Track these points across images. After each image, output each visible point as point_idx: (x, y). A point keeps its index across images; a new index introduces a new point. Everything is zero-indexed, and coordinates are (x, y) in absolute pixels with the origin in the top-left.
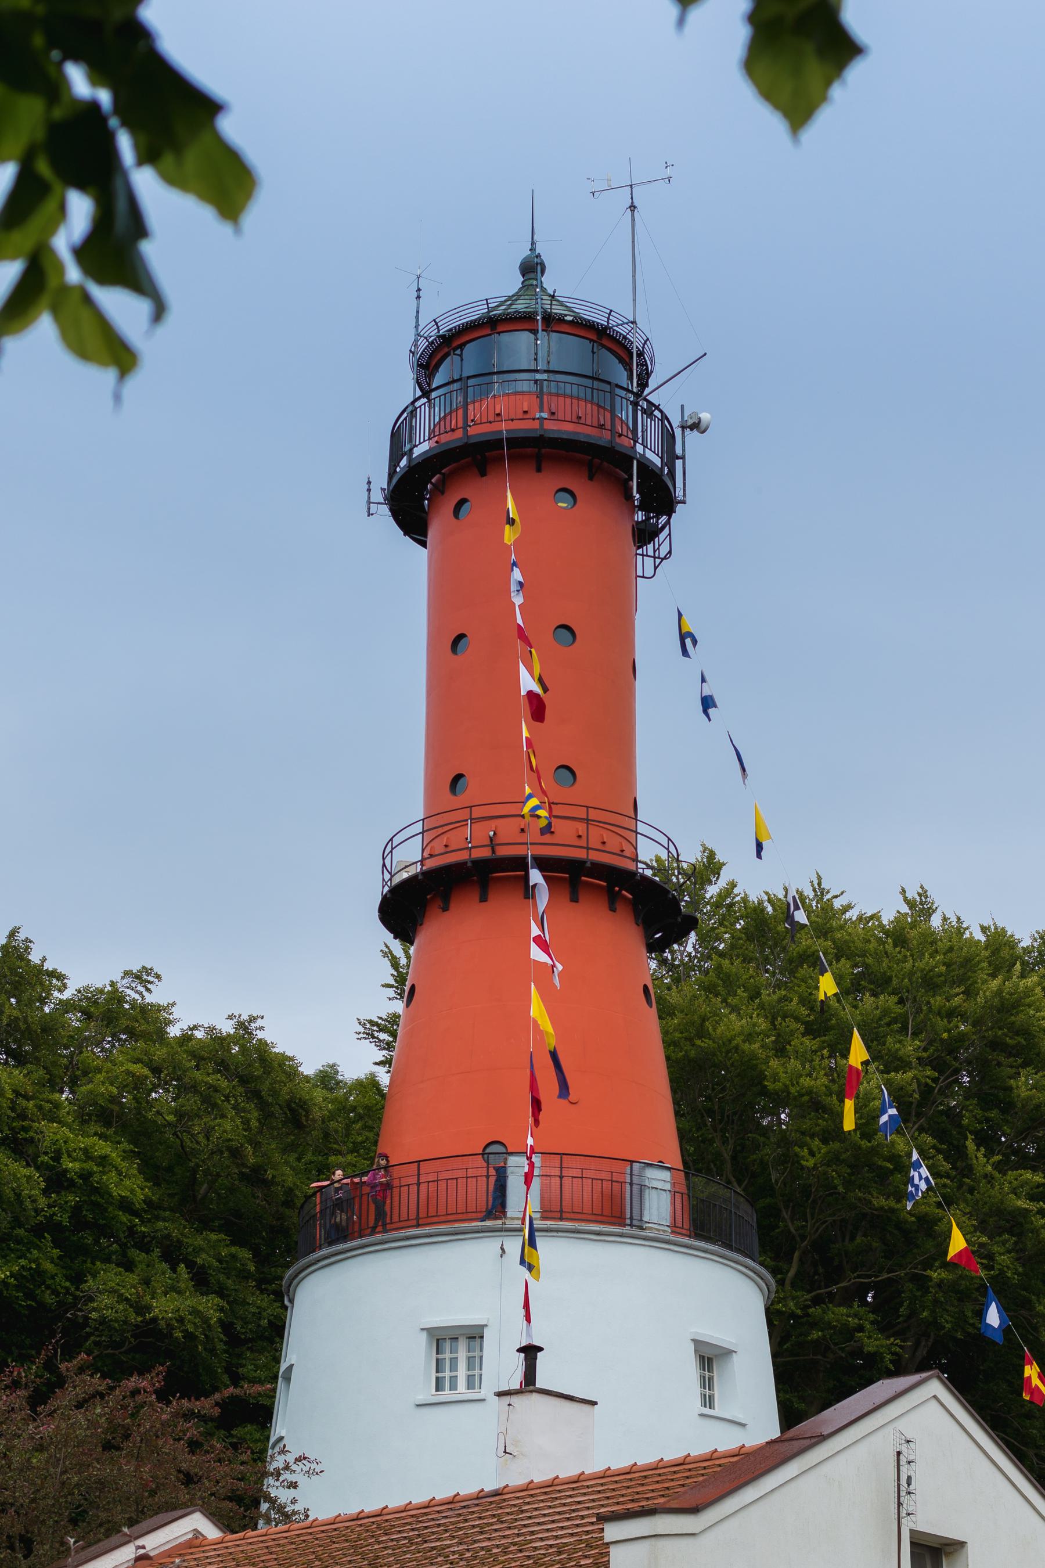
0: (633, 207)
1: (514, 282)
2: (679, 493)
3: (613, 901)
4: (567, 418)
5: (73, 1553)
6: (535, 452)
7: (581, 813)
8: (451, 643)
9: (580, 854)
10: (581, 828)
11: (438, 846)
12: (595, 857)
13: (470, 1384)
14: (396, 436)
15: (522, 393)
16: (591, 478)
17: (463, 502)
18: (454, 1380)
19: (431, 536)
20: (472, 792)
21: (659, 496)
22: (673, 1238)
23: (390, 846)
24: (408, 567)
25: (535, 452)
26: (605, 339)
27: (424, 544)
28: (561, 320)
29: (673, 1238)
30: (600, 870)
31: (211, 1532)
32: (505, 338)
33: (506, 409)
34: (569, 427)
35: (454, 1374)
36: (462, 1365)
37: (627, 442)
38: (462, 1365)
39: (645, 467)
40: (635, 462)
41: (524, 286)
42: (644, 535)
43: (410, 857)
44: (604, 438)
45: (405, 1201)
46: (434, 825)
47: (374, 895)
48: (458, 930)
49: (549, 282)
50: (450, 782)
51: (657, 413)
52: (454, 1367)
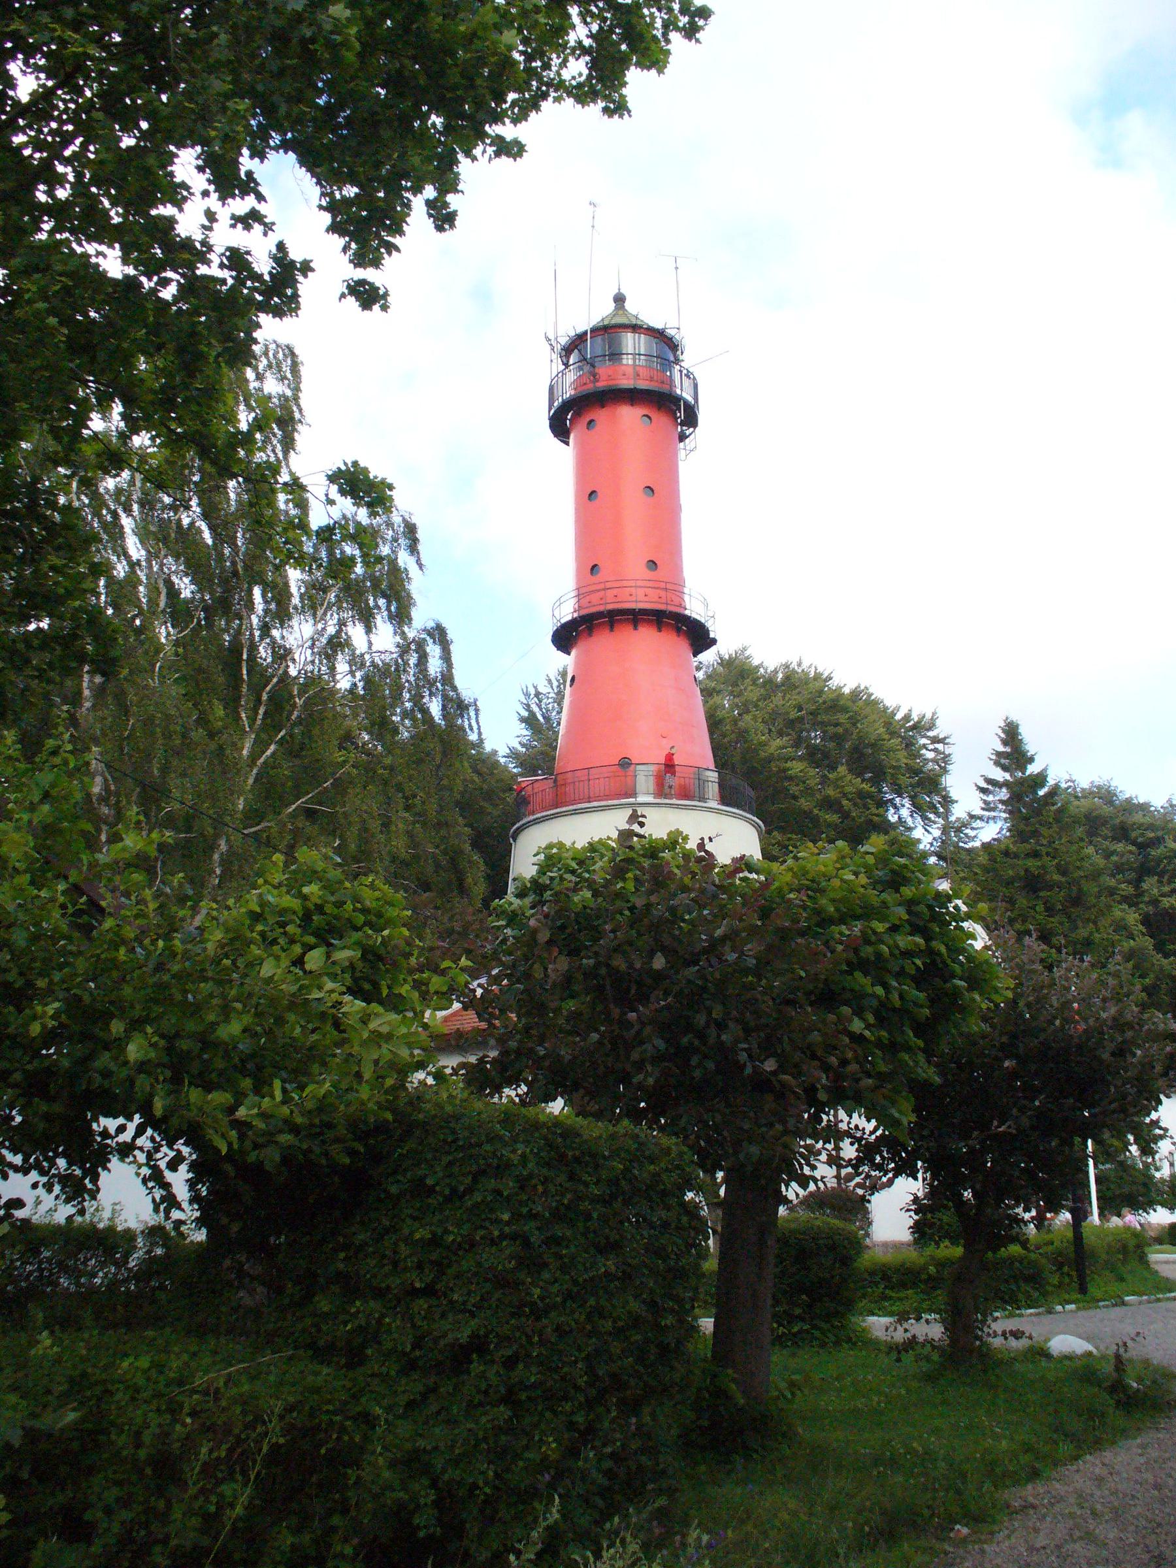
1: (611, 306)
2: (297, 415)
3: (678, 631)
6: (633, 396)
7: (663, 585)
8: (589, 495)
10: (663, 593)
11: (585, 601)
14: (551, 389)
17: (591, 421)
20: (603, 575)
21: (691, 419)
23: (560, 602)
25: (633, 396)
26: (659, 335)
27: (567, 444)
28: (640, 327)
30: (600, 615)
39: (686, 404)
41: (616, 309)
42: (682, 437)
43: (567, 613)
46: (581, 594)
48: (602, 643)
50: (591, 569)
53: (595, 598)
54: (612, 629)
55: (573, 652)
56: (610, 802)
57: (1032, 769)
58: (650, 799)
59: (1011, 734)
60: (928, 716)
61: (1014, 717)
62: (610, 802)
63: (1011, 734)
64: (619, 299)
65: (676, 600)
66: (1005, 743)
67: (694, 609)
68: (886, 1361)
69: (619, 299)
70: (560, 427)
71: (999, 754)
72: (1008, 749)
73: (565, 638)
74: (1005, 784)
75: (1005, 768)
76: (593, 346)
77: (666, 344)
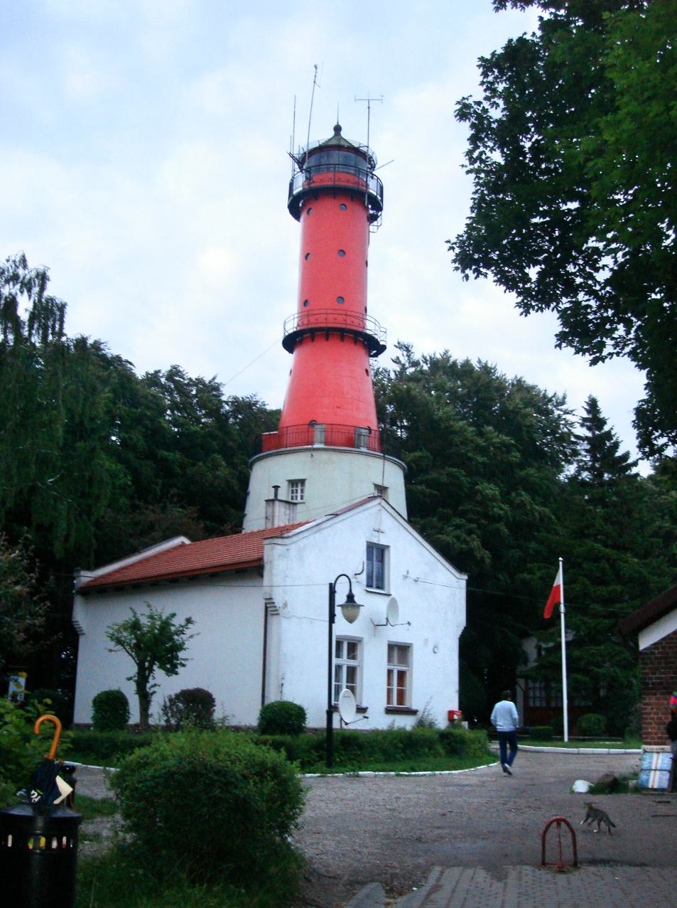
0: (369, 107)
1: (332, 133)
4: (345, 180)
5: (643, 561)
9: (343, 326)
10: (325, 316)
12: (349, 327)
13: (302, 498)
15: (350, 173)
16: (334, 198)
17: (310, 209)
18: (297, 497)
19: (302, 219)
21: (378, 206)
22: (326, 447)
24: (295, 229)
27: (299, 221)
29: (326, 447)
30: (351, 331)
31: (187, 541)
32: (331, 152)
33: (325, 179)
34: (346, 184)
35: (352, 663)
36: (299, 491)
37: (364, 188)
38: (299, 491)
40: (366, 196)
43: (292, 327)
44: (355, 187)
45: (290, 438)
47: (281, 338)
49: (343, 134)
51: (375, 177)
52: (297, 493)
53: (312, 319)
54: (313, 340)
55: (295, 353)
56: (298, 448)
57: (606, 428)
58: (322, 446)
59: (593, 406)
60: (560, 395)
61: (594, 396)
62: (298, 448)
63: (593, 406)
64: (338, 129)
65: (356, 322)
66: (588, 412)
67: (370, 328)
68: (568, 791)
69: (338, 129)
70: (295, 210)
71: (584, 419)
72: (590, 416)
73: (291, 343)
74: (587, 438)
75: (589, 429)
76: (312, 159)
77: (360, 158)
